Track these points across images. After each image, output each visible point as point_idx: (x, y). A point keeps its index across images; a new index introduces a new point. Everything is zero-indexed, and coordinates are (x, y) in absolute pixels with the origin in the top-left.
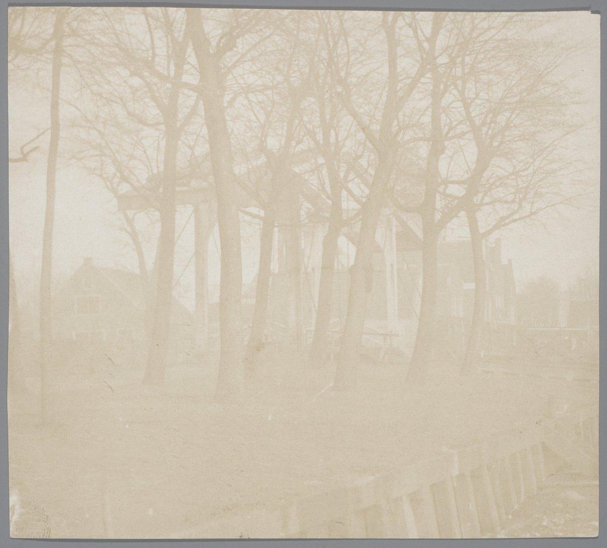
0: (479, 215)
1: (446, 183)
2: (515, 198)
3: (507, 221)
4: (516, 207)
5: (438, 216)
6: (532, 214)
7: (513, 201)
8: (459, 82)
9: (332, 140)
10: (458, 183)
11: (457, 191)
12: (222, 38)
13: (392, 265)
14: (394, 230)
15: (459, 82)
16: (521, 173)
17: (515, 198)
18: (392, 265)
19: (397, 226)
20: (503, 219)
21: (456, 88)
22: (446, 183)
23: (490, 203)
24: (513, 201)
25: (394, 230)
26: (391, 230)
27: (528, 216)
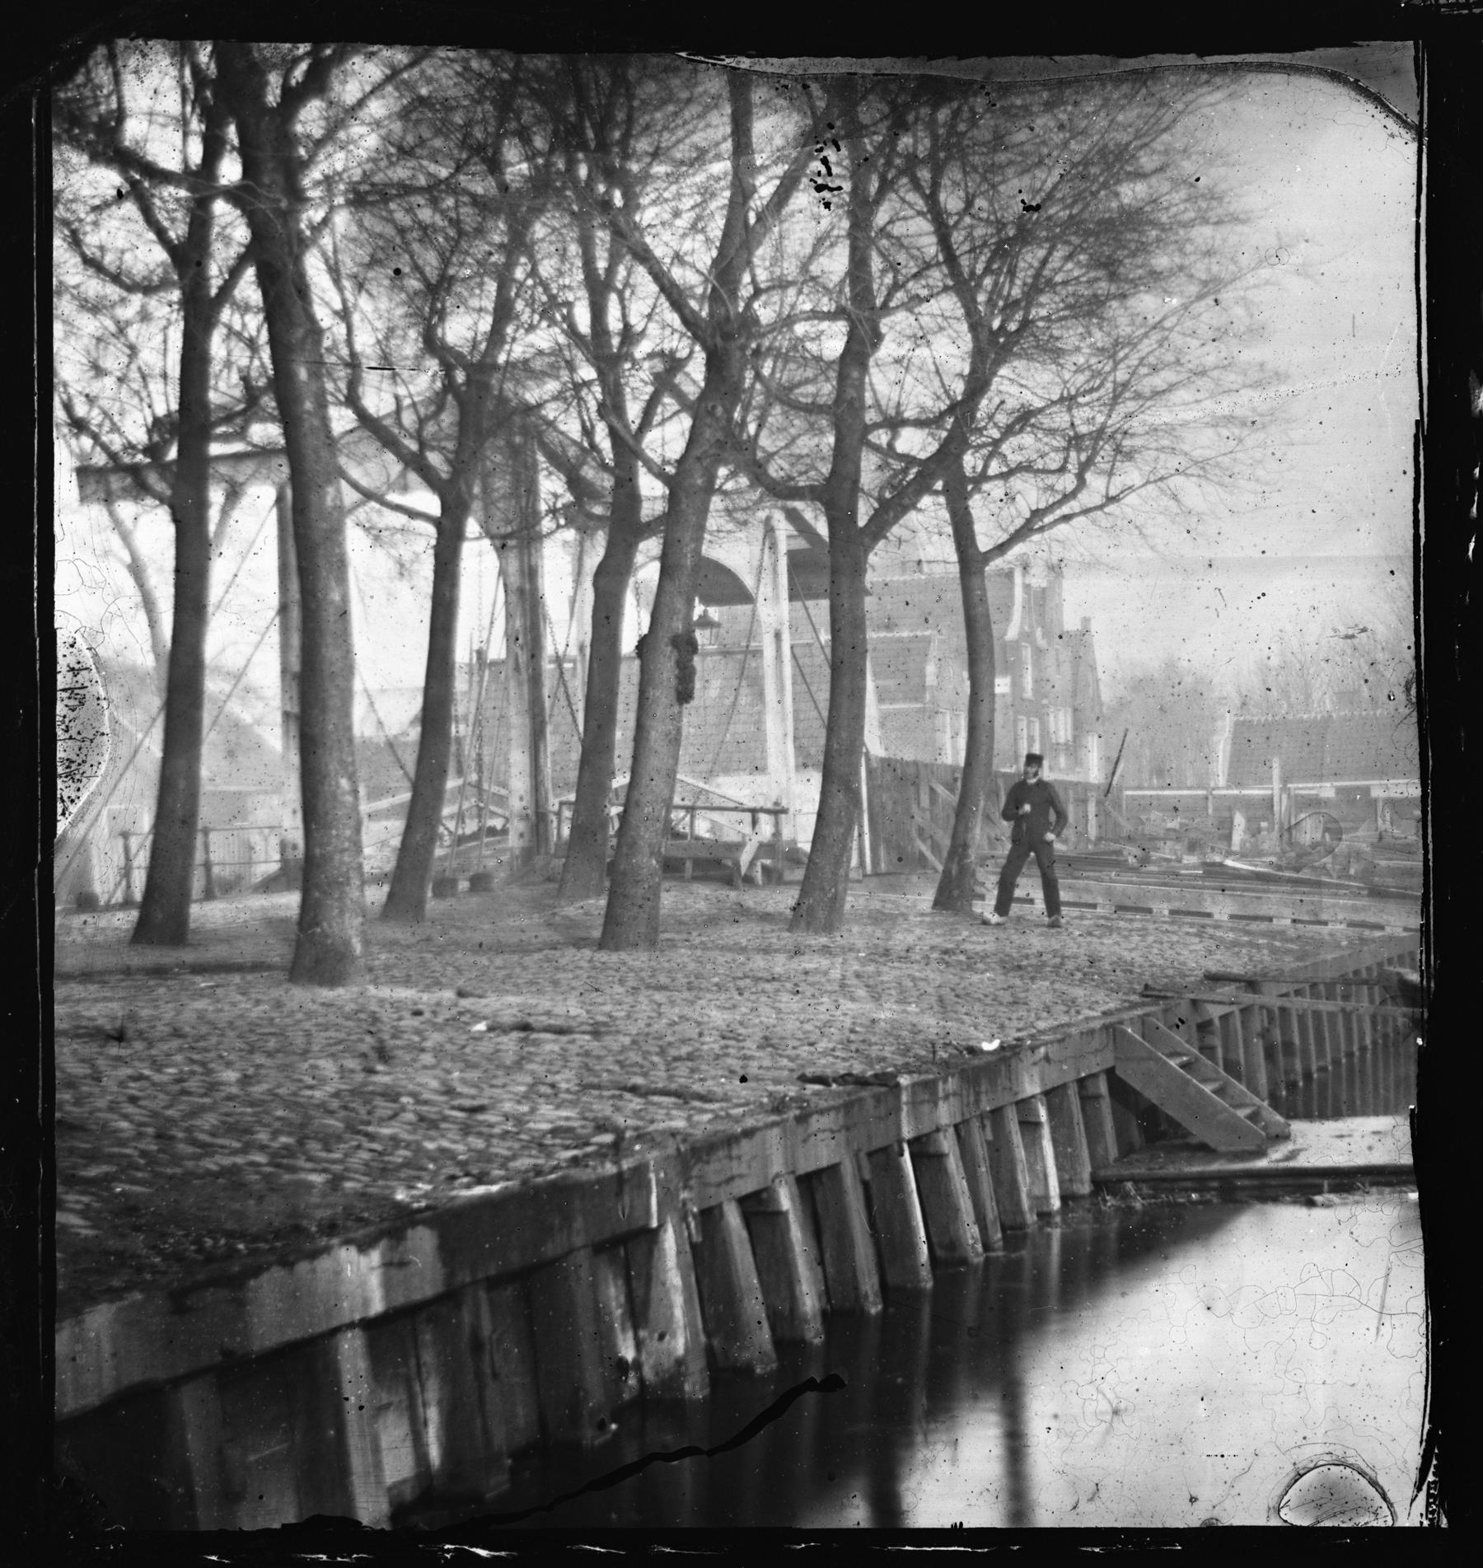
0: (976, 504)
1: (895, 423)
2: (1066, 460)
3: (1048, 519)
4: (1068, 482)
5: (864, 512)
6: (1111, 499)
7: (1062, 470)
8: (924, 174)
9: (614, 323)
10: (919, 423)
11: (915, 443)
12: (1156, 394)
13: (778, 636)
14: (783, 547)
15: (924, 174)
16: (1081, 400)
17: (1066, 460)
18: (778, 636)
19: (789, 537)
20: (1037, 514)
21: (916, 185)
22: (895, 423)
23: (1004, 476)
24: (1062, 470)
25: (783, 547)
26: (773, 547)
27: (1101, 507)
